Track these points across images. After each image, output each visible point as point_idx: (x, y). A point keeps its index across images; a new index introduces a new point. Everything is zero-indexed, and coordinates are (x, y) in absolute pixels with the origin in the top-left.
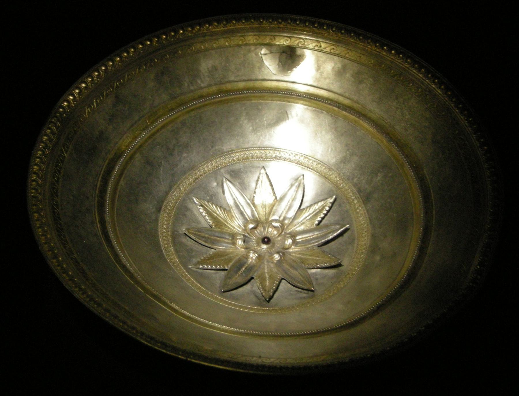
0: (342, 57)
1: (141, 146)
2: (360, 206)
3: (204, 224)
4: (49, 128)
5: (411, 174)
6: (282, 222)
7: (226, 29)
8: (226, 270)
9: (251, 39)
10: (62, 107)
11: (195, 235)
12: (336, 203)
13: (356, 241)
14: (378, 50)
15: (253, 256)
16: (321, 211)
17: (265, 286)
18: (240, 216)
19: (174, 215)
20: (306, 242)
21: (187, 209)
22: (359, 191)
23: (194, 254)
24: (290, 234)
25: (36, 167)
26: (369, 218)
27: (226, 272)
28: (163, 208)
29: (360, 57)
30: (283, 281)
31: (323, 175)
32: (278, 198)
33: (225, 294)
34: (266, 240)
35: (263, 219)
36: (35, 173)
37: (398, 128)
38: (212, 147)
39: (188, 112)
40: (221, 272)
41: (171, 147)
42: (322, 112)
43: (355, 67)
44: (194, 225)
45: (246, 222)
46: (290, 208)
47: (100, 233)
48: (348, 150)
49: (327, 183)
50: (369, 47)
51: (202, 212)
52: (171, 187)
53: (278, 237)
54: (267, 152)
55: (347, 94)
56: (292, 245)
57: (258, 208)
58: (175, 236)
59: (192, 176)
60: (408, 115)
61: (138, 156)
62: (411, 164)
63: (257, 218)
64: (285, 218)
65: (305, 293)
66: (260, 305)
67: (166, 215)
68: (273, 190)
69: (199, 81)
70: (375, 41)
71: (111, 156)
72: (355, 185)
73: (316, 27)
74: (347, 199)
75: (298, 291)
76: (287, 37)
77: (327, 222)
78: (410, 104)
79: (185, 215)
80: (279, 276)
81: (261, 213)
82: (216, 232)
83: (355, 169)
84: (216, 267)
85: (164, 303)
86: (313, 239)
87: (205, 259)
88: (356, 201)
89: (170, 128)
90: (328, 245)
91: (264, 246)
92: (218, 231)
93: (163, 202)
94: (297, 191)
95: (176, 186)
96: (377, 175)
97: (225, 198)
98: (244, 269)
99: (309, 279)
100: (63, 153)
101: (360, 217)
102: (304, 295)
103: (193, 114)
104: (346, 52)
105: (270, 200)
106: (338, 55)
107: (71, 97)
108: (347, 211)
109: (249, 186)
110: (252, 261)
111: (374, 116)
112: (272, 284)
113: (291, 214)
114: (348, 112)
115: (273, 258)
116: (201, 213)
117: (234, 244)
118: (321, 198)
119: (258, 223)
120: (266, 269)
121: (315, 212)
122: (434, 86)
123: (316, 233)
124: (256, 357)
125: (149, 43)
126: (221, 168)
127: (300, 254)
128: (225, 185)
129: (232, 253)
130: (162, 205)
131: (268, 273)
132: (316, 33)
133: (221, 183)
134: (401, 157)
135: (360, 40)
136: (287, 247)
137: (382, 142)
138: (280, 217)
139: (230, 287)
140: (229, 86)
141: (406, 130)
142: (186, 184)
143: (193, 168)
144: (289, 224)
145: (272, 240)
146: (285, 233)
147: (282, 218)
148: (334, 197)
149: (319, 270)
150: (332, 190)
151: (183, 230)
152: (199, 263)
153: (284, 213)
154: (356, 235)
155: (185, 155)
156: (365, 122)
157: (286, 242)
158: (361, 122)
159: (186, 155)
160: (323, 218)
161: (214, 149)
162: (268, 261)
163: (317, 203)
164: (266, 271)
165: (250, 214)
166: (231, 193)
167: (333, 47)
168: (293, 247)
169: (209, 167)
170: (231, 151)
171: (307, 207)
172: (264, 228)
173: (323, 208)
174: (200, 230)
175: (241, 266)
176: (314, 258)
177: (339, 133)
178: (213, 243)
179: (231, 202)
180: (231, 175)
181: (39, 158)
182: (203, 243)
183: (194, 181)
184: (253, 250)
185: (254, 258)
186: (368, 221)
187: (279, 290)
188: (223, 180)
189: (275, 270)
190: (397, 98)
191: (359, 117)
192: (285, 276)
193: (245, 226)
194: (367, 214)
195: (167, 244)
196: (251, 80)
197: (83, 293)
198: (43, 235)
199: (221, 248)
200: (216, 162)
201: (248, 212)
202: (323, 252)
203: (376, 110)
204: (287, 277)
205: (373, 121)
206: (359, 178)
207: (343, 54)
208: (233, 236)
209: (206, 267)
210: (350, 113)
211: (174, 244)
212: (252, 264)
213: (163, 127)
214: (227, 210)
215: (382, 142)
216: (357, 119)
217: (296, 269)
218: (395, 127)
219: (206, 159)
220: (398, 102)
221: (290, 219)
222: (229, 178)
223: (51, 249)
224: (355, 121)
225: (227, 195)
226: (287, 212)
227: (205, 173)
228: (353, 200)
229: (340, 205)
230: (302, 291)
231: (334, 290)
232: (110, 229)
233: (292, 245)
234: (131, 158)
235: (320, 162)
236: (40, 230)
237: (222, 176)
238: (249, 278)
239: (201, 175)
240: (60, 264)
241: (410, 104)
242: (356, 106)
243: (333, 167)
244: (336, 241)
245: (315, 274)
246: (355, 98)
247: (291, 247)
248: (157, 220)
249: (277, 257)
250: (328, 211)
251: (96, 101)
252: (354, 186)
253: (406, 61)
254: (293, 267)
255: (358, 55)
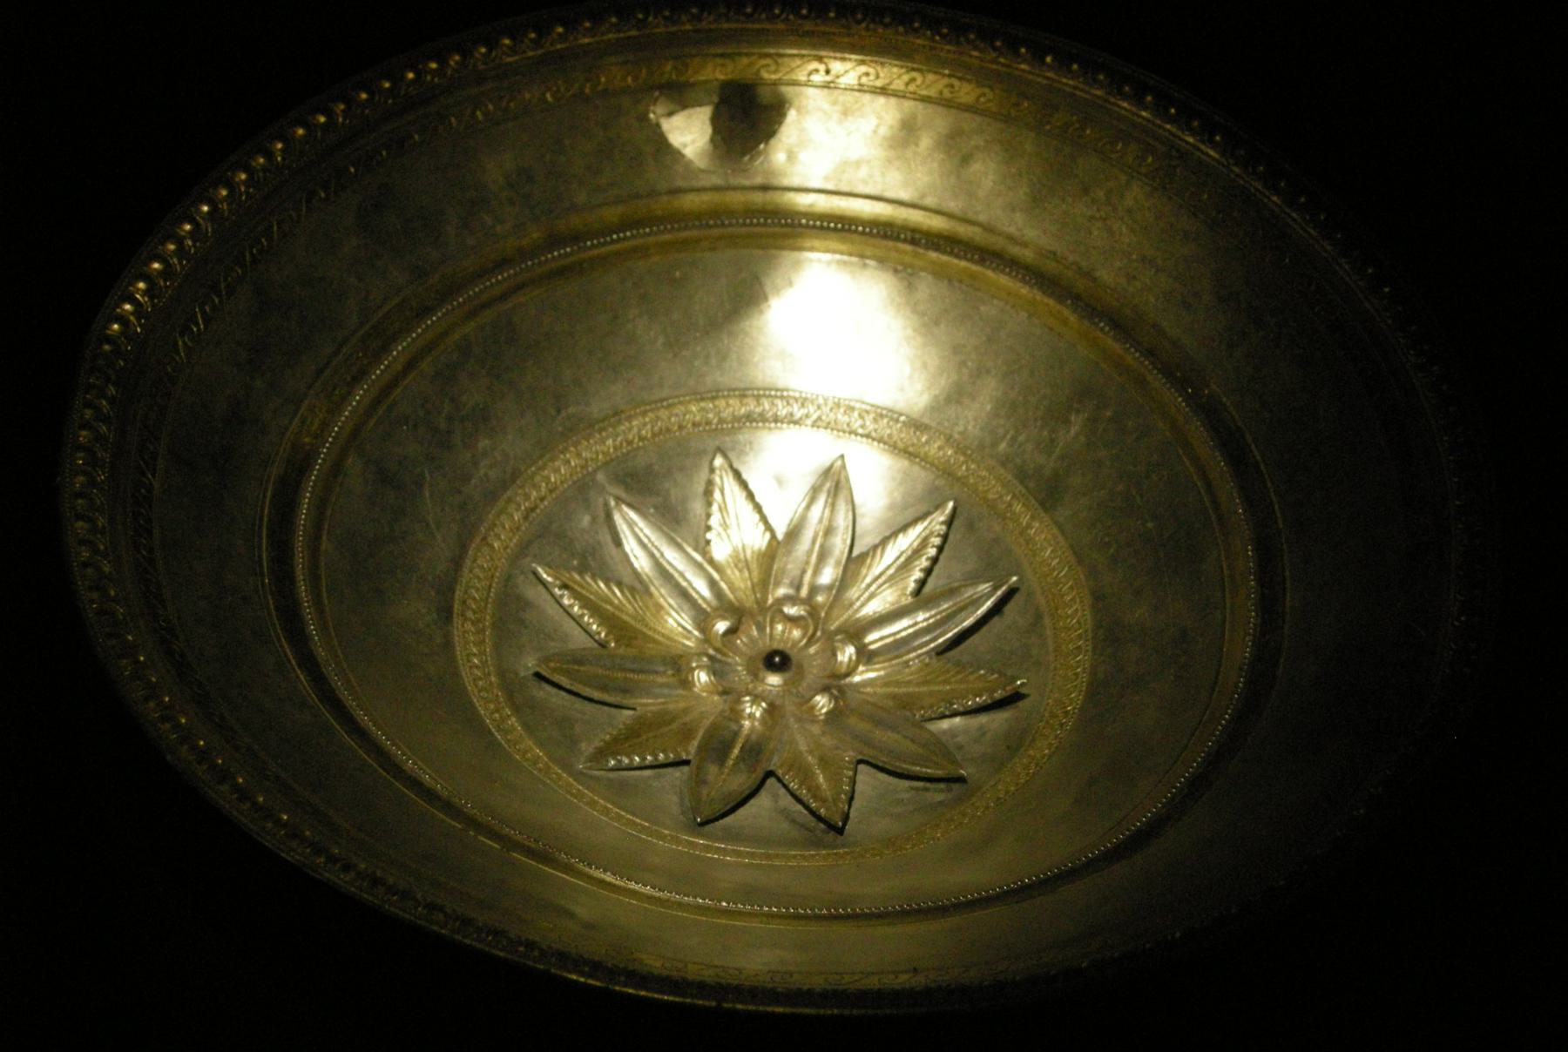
0: (896, 94)
1: (355, 433)
2: (1033, 518)
3: (579, 640)
4: (88, 405)
5: (1176, 401)
6: (809, 601)
7: (539, 52)
8: (687, 763)
9: (614, 75)
10: (109, 340)
11: (567, 673)
12: (956, 523)
13: (1047, 621)
14: (1002, 60)
15: (753, 711)
16: (917, 552)
17: (818, 787)
18: (680, 600)
19: (494, 625)
20: (900, 646)
21: (525, 604)
22: (1022, 475)
23: (578, 729)
24: (839, 631)
25: (80, 524)
26: (1072, 547)
27: (685, 769)
28: (457, 607)
29: (952, 86)
30: (861, 767)
31: (900, 445)
32: (780, 536)
33: (708, 828)
34: (777, 660)
35: (750, 602)
36: (82, 542)
37: (1105, 275)
38: (559, 412)
39: (473, 314)
40: (669, 770)
41: (443, 425)
42: (865, 265)
43: (941, 121)
44: (554, 646)
45: (703, 620)
46: (823, 556)
47: (314, 698)
48: (963, 364)
49: (916, 469)
50: (975, 53)
51: (572, 606)
52: (464, 548)
53: (810, 643)
54: (722, 403)
55: (930, 201)
56: (858, 662)
57: (729, 572)
58: (511, 688)
59: (519, 505)
60: (1125, 233)
61: (353, 464)
62: (1168, 372)
63: (730, 603)
64: (814, 590)
65: (941, 791)
66: (818, 844)
67: (468, 626)
68: (758, 508)
69: (489, 220)
70: (987, 36)
71: (275, 471)
72: (1004, 462)
73: (805, 17)
74: (992, 505)
75: (917, 789)
76: (722, 55)
77: (941, 582)
78: (1129, 202)
79: (522, 622)
80: (849, 756)
81: (739, 584)
82: (623, 657)
83: (997, 416)
84: (656, 759)
85: (568, 869)
86: (917, 635)
87: (616, 740)
88: (1018, 508)
89: (425, 365)
90: (963, 646)
91: (774, 680)
92: (628, 657)
93: (452, 590)
94: (833, 505)
95: (478, 540)
96: (1067, 422)
97: (626, 556)
98: (736, 751)
99: (940, 748)
100: (143, 474)
101: (1044, 546)
102: (940, 797)
103: (487, 316)
104: (906, 78)
105: (757, 540)
106: (883, 91)
107: (128, 307)
108: (996, 541)
109: (686, 511)
110: (752, 728)
111: (1028, 255)
112: (835, 779)
113: (828, 576)
114: (944, 252)
115: (813, 708)
116: (566, 609)
117: (686, 684)
118: (910, 514)
119: (738, 614)
120: (802, 741)
121: (902, 559)
122: (1191, 140)
123: (921, 616)
124: (906, 972)
125: (322, 119)
126: (595, 471)
127: (887, 684)
128: (617, 518)
129: (685, 711)
130: (452, 599)
131: (811, 752)
132: (811, 34)
133: (602, 515)
134: (1132, 358)
135: (943, 37)
136: (844, 669)
137: (1065, 322)
138: (798, 588)
139: (719, 808)
140: (576, 221)
141: (1131, 278)
142: (503, 533)
143: (512, 478)
144: (832, 606)
145: (794, 660)
146: (824, 632)
147: (804, 592)
148: (951, 505)
149: (957, 720)
150: (937, 488)
151: (530, 663)
152: (601, 754)
153: (809, 572)
154: (1043, 602)
155: (484, 443)
156: (1002, 272)
157: (840, 658)
158: (990, 273)
159: (487, 442)
160: (928, 572)
161: (564, 413)
162: (799, 720)
163: (904, 528)
164: (803, 747)
165: (706, 592)
166: (638, 539)
167: (863, 69)
168: (861, 668)
169: (560, 471)
170: (616, 414)
171: (875, 547)
172: (761, 629)
173: (924, 543)
174: (578, 659)
175: (726, 747)
176: (936, 688)
177: (929, 323)
178: (625, 691)
179: (641, 562)
180: (628, 488)
181: (79, 495)
182: (596, 695)
183: (526, 518)
184: (749, 694)
185: (758, 714)
186: (1073, 559)
187: (857, 795)
188: (606, 504)
189: (827, 741)
190: (1086, 191)
191: (982, 262)
192: (869, 754)
193: (702, 630)
194: (1061, 538)
195: (497, 711)
196: (638, 196)
197: (347, 868)
198: (164, 719)
199: (648, 704)
200: (579, 455)
201: (701, 587)
202: (958, 664)
203: (1028, 232)
204: (872, 752)
205: (1027, 268)
206: (1014, 439)
207: (899, 85)
208: (678, 665)
209: (626, 761)
210: (951, 253)
211: (517, 710)
212: (754, 737)
213: (410, 366)
214: (637, 587)
215: (1065, 322)
216: (975, 268)
217: (893, 728)
218: (1098, 274)
219: (546, 448)
220: (1093, 201)
221: (830, 588)
222: (623, 495)
223: (203, 756)
224: (973, 276)
225: (630, 545)
226: (817, 571)
227: (551, 491)
228: (1010, 505)
229: (971, 526)
230: (928, 785)
231: (1027, 767)
232: (336, 682)
233: (858, 662)
234: (336, 469)
235: (881, 413)
236: (152, 704)
237: (602, 490)
238: (760, 773)
239: (542, 499)
240: (244, 795)
241: (1129, 202)
242: (963, 230)
243: (926, 420)
244: (984, 629)
245: (952, 733)
246: (953, 205)
247: (856, 668)
248: (448, 645)
249: (822, 702)
250: (940, 549)
251: (204, 313)
252: (1003, 464)
253: (1095, 81)
254: (879, 723)
255: (945, 81)
